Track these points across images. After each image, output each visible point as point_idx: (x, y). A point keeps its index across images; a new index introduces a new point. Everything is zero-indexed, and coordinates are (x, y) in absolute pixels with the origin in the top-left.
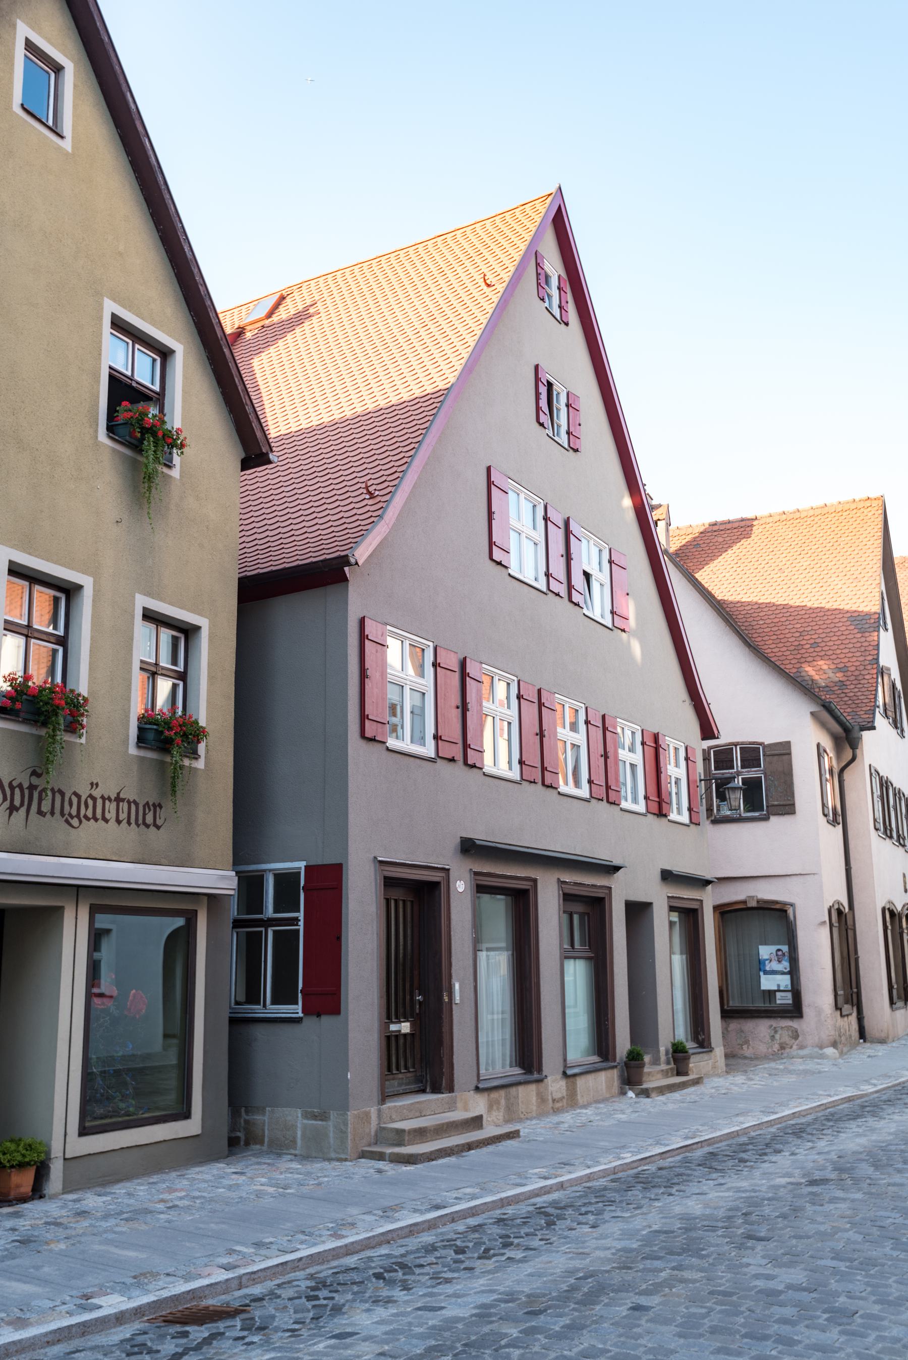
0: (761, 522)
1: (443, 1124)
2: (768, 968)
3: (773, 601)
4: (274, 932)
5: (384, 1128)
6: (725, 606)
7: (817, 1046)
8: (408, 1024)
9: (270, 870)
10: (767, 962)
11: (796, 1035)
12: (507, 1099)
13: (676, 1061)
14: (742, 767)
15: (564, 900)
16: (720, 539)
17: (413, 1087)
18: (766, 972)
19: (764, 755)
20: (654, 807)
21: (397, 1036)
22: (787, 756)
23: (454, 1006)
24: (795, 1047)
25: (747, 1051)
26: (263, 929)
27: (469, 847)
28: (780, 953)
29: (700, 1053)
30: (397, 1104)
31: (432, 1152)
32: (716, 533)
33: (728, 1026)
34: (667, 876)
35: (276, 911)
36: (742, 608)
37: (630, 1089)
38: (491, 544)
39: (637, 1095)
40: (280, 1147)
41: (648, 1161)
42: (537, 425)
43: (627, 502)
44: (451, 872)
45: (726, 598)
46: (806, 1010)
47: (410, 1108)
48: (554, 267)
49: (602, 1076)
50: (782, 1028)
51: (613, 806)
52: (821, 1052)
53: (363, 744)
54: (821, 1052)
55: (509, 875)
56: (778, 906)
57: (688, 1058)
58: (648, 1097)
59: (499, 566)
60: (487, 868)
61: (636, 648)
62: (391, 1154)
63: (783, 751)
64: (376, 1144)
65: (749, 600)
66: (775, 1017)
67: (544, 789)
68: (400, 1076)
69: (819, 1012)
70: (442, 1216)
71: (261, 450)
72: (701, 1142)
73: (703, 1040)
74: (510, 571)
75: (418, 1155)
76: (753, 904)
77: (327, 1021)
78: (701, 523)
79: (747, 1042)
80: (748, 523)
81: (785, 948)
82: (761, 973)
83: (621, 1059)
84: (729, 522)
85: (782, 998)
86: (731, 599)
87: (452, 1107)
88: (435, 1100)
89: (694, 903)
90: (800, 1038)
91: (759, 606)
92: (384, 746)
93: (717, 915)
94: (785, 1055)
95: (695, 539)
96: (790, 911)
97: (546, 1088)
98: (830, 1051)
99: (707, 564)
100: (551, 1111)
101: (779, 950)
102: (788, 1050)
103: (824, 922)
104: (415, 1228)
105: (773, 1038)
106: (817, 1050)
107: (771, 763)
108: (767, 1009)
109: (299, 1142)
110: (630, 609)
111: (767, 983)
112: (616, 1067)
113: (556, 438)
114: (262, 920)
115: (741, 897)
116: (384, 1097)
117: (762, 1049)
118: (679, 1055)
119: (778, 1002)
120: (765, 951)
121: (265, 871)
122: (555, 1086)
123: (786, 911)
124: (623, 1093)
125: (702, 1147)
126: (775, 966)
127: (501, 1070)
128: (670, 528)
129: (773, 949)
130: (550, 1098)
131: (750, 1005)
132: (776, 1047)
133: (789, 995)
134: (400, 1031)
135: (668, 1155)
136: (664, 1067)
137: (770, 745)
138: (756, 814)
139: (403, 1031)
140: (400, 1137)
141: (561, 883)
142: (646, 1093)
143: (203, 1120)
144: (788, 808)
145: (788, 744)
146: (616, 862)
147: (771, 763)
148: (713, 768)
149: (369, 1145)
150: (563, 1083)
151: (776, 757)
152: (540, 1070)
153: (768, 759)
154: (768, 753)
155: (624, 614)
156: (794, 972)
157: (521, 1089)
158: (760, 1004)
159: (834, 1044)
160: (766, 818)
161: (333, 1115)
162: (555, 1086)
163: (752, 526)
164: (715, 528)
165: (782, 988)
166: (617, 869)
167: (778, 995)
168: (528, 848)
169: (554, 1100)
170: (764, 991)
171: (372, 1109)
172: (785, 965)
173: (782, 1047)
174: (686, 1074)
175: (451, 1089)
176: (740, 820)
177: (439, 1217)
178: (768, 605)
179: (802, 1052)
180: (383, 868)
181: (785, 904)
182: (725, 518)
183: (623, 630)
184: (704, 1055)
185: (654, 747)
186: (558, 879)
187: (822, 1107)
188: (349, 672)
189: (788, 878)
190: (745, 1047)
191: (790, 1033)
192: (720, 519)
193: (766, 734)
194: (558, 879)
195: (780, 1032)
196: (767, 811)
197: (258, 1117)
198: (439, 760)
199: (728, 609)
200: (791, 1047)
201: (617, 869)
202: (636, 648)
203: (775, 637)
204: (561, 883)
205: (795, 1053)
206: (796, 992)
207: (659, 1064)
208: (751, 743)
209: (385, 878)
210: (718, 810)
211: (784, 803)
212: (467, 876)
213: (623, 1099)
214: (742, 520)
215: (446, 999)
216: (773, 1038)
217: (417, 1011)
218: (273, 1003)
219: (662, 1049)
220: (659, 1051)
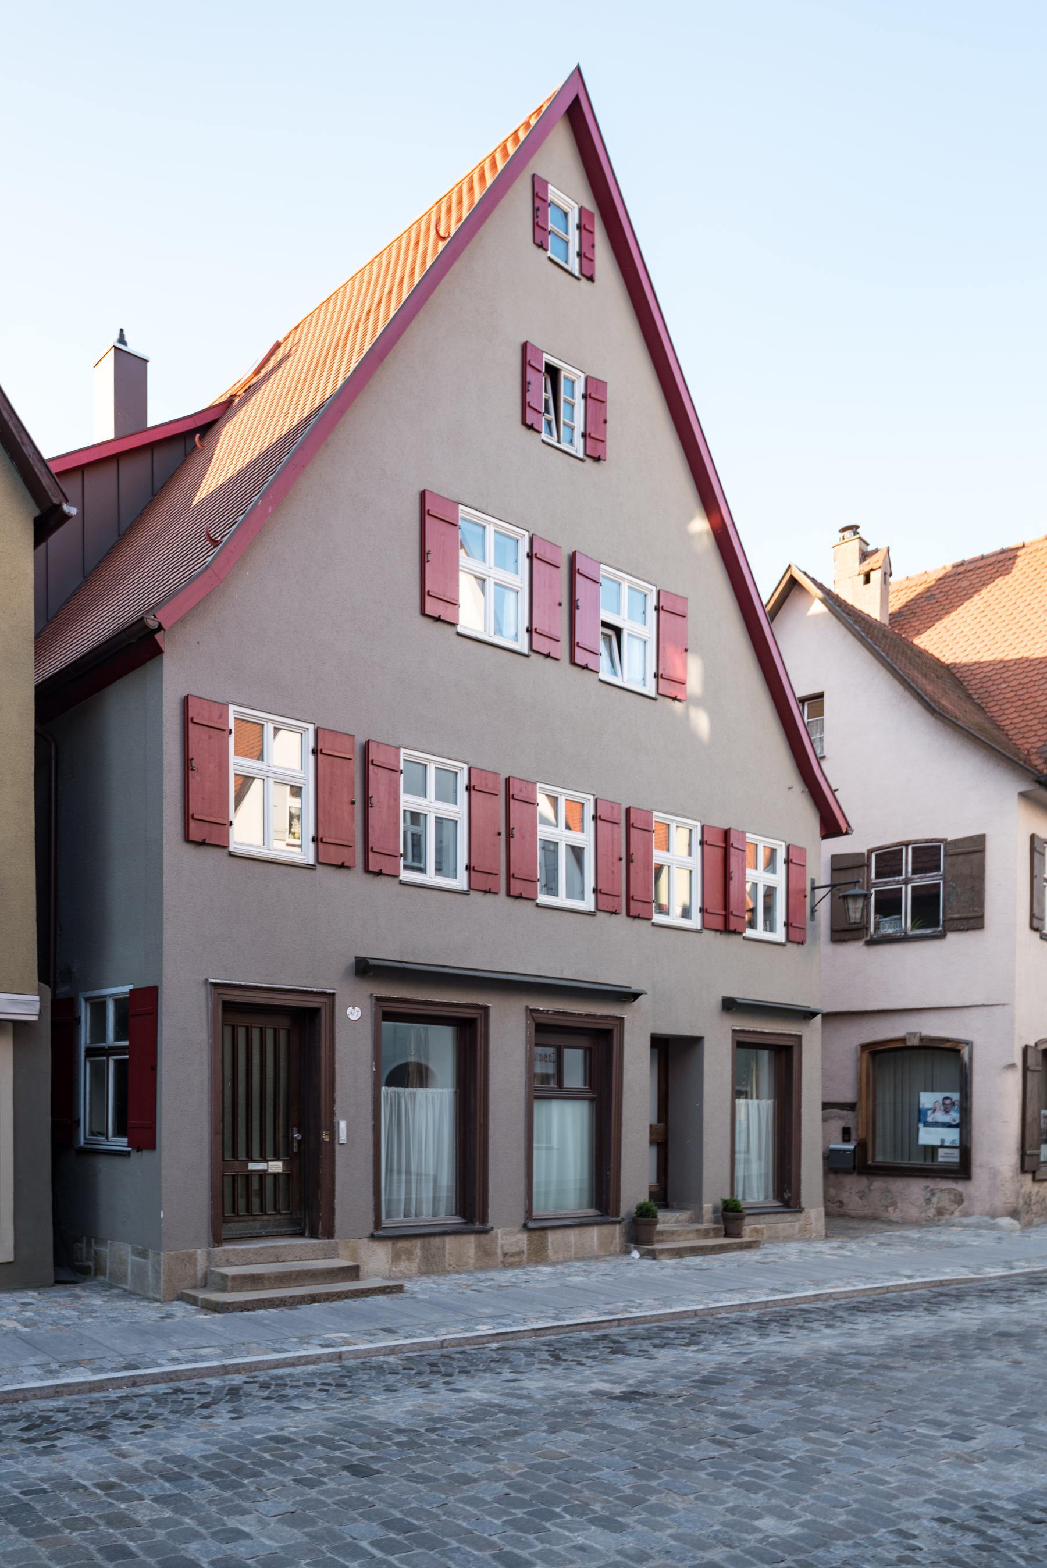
0: (1030, 550)
1: (291, 1272)
2: (930, 1119)
3: (1026, 655)
4: (116, 1061)
5: (212, 1272)
6: (955, 671)
7: (987, 1214)
8: (280, 1164)
9: (110, 996)
10: (929, 1112)
11: (959, 1200)
12: (424, 1248)
13: (725, 1220)
14: (914, 872)
15: (537, 1031)
16: (965, 583)
17: (289, 1230)
18: (927, 1124)
19: (945, 856)
20: (718, 922)
21: (261, 1176)
22: (978, 855)
23: (337, 1147)
24: (957, 1213)
25: (893, 1214)
26: (105, 1058)
27: (364, 969)
28: (948, 1102)
29: (783, 1212)
30: (237, 1247)
31: (247, 1302)
32: (960, 577)
33: (871, 1184)
34: (729, 1005)
35: (117, 1039)
36: (980, 670)
37: (635, 1248)
38: (423, 593)
39: (642, 1256)
40: (112, 1283)
41: (510, 1336)
42: (523, 429)
43: (700, 525)
44: (337, 998)
45: (958, 661)
46: (976, 1171)
47: (258, 1252)
48: (569, 196)
49: (594, 1234)
50: (942, 1190)
51: (637, 922)
52: (992, 1222)
53: (190, 850)
54: (992, 1222)
55: (437, 1005)
56: (948, 1045)
57: (742, 1218)
58: (654, 1259)
59: (439, 624)
60: (383, 991)
61: (701, 721)
62: (203, 1299)
63: (973, 849)
64: (205, 1286)
65: (991, 658)
66: (933, 1177)
67: (510, 901)
68: (265, 1217)
69: (994, 1174)
70: (113, 1379)
71: (51, 501)
72: (619, 1320)
73: (790, 1199)
74: (460, 629)
75: (225, 1303)
76: (915, 1042)
77: (146, 1154)
78: (942, 565)
79: (894, 1204)
80: (1011, 554)
81: (956, 1096)
82: (921, 1125)
83: (629, 1214)
84: (983, 558)
85: (946, 1155)
86: (965, 660)
87: (332, 1253)
88: (301, 1245)
89: (788, 1039)
90: (965, 1204)
91: (1004, 665)
92: (225, 851)
93: (866, 1055)
94: (943, 1222)
95: (928, 589)
96: (965, 1052)
97: (495, 1240)
98: (1006, 1221)
99: (940, 619)
100: (501, 1266)
101: (947, 1098)
102: (947, 1217)
103: (1012, 1066)
104: (66, 1389)
105: (928, 1201)
106: (987, 1218)
107: (953, 865)
108: (927, 1167)
109: (129, 1277)
110: (694, 674)
111: (927, 1137)
112: (619, 1222)
113: (563, 446)
114: (103, 1048)
115: (899, 1034)
116: (218, 1239)
117: (913, 1212)
118: (731, 1216)
119: (940, 1159)
120: (927, 1099)
121: (105, 996)
122: (508, 1237)
123: (959, 1051)
124: (628, 1252)
125: (619, 1326)
126: (940, 1117)
127: (430, 1217)
128: (891, 579)
129: (939, 1096)
130: (499, 1251)
131: (905, 1162)
132: (931, 1212)
133: (956, 1152)
134: (266, 1171)
135: (551, 1331)
136: (706, 1225)
137: (955, 842)
138: (929, 931)
139: (270, 1171)
140: (224, 1283)
141: (532, 1012)
142: (653, 1255)
143: (15, 1247)
144: (973, 920)
145: (981, 839)
146: (635, 988)
147: (953, 865)
148: (873, 875)
149: (194, 1287)
150: (523, 1238)
151: (961, 857)
152: (484, 1219)
153: (949, 859)
154: (950, 852)
155: (677, 675)
156: (964, 1124)
157: (449, 1241)
158: (918, 1162)
159: (1014, 1214)
160: (941, 936)
161: (151, 1253)
162: (508, 1237)
163: (1016, 557)
164: (961, 569)
165: (946, 1144)
166: (635, 996)
167: (941, 1152)
168: (476, 970)
169: (505, 1255)
170: (925, 1147)
171: (199, 1251)
172: (954, 1116)
173: (940, 1212)
174: (738, 1235)
175: (330, 1234)
176: (903, 939)
177: (108, 1379)
178: (1016, 662)
179: (965, 1221)
180: (219, 991)
181: (959, 1042)
182: (977, 554)
183: (675, 699)
184: (788, 1215)
185: (722, 851)
186: (527, 1007)
187: (879, 1291)
188: (165, 763)
189: (965, 1010)
190: (891, 1209)
191: (952, 1197)
192: (968, 556)
193: (951, 828)
194: (527, 1007)
195: (938, 1195)
196: (944, 926)
197: (102, 1249)
198: (319, 867)
199: (958, 675)
200: (952, 1213)
201: (635, 996)
202: (701, 721)
203: (1020, 703)
204: (532, 1012)
205: (957, 1220)
206: (965, 1150)
207: (702, 1223)
208: (927, 841)
209: (224, 1003)
210: (877, 928)
211: (969, 915)
212: (368, 1003)
213: (625, 1260)
214: (1003, 552)
215: (326, 1138)
216: (928, 1201)
217: (295, 1150)
218: (114, 1136)
219: (707, 1207)
220: (701, 1208)
